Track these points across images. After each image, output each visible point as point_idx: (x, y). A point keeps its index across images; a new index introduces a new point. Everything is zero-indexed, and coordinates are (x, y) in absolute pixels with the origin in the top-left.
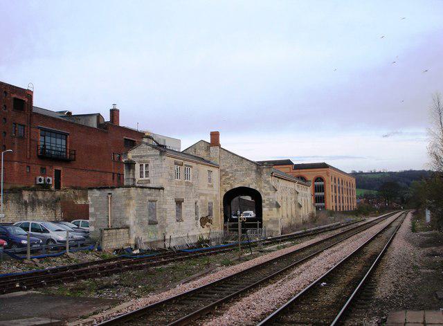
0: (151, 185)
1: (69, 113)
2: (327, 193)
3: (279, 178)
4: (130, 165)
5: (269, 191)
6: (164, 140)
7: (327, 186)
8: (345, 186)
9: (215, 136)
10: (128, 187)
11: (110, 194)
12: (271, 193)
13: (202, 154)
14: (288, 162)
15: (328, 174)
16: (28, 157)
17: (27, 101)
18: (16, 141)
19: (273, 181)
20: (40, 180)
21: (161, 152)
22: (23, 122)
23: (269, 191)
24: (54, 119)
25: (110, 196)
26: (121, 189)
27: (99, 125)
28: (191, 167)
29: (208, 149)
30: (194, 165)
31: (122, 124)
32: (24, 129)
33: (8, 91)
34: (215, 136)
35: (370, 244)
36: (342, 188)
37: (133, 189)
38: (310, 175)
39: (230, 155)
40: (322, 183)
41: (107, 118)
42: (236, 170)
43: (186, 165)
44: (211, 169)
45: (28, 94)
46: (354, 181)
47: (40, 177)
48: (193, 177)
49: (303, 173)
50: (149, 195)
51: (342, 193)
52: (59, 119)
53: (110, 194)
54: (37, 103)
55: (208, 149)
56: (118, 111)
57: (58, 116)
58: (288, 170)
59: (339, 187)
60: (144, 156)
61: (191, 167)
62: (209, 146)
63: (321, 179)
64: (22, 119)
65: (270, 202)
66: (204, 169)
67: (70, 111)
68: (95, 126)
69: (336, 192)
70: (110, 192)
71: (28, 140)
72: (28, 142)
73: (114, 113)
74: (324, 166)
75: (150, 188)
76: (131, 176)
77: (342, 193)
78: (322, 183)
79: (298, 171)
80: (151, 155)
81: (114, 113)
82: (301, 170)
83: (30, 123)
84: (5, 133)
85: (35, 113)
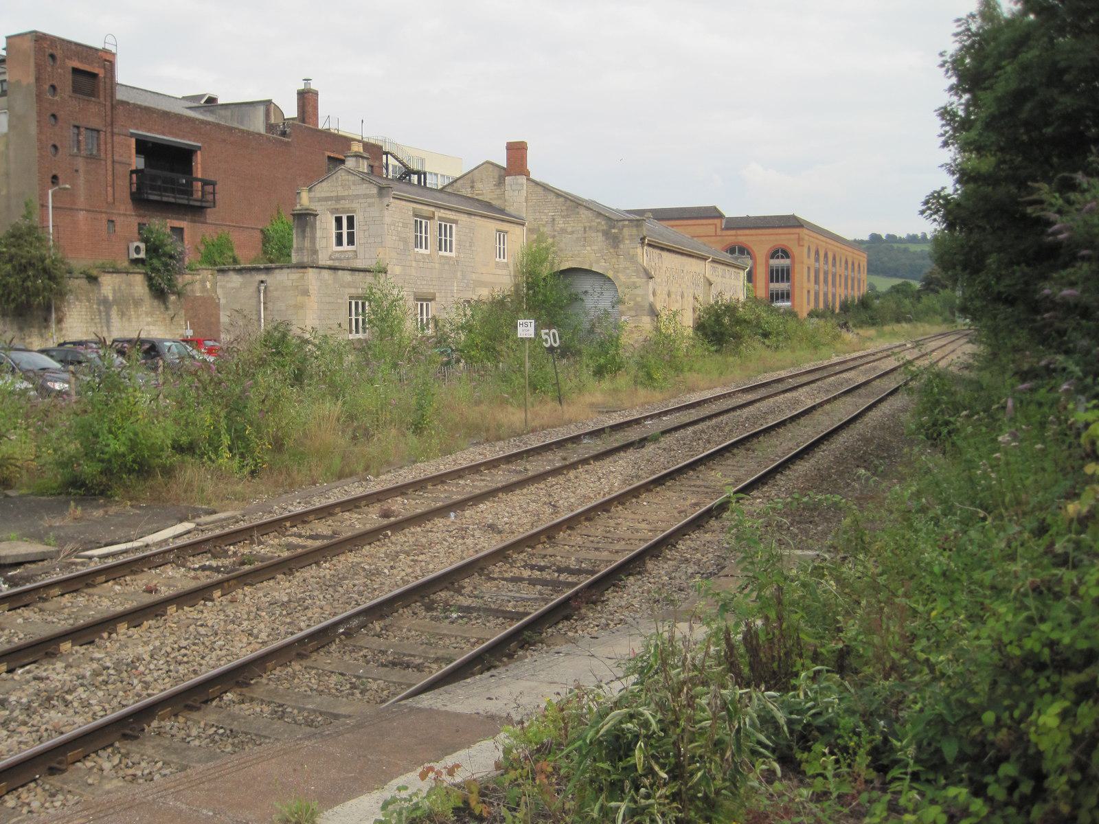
0: (359, 264)
1: (211, 100)
2: (796, 284)
3: (662, 249)
4: (304, 219)
5: (635, 279)
6: (423, 160)
7: (797, 267)
8: (840, 270)
9: (517, 151)
10: (302, 266)
11: (262, 282)
12: (640, 281)
13: (486, 191)
14: (711, 214)
15: (799, 239)
16: (110, 199)
17: (102, 75)
18: (80, 164)
19: (646, 257)
20: (137, 250)
21: (381, 189)
22: (96, 123)
23: (635, 279)
24: (166, 115)
25: (262, 288)
26: (286, 271)
27: (270, 128)
28: (455, 222)
29: (500, 182)
30: (463, 218)
31: (322, 125)
32: (98, 138)
33: (59, 53)
34: (517, 151)
35: (802, 421)
36: (834, 276)
37: (311, 273)
38: (761, 244)
39: (551, 197)
40: (784, 262)
41: (290, 110)
42: (563, 231)
43: (441, 219)
44: (505, 226)
45: (106, 60)
46: (863, 259)
47: (136, 244)
48: (459, 243)
49: (744, 238)
50: (349, 285)
51: (834, 285)
52: (179, 118)
53: (262, 282)
54: (125, 75)
55: (500, 182)
56: (316, 93)
57: (180, 109)
58: (711, 230)
59: (826, 273)
60: (343, 198)
61: (455, 222)
62: (503, 174)
63: (785, 254)
64: (93, 115)
65: (637, 304)
66: (487, 228)
67: (212, 92)
68: (262, 130)
69: (817, 282)
70: (263, 277)
71: (109, 162)
72: (110, 168)
73: (307, 99)
74: (792, 223)
75: (353, 270)
76: (307, 244)
77: (834, 285)
78: (784, 262)
79: (733, 232)
80: (357, 197)
81: (307, 99)
82: (740, 232)
83: (112, 124)
84: (55, 146)
85: (124, 103)
